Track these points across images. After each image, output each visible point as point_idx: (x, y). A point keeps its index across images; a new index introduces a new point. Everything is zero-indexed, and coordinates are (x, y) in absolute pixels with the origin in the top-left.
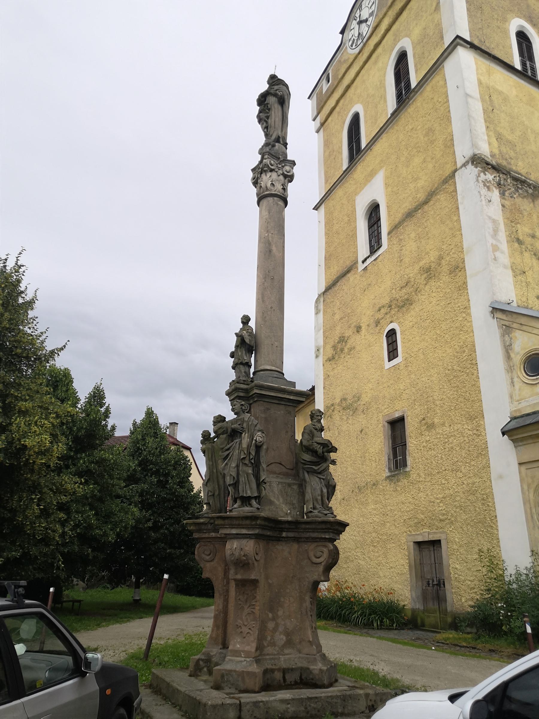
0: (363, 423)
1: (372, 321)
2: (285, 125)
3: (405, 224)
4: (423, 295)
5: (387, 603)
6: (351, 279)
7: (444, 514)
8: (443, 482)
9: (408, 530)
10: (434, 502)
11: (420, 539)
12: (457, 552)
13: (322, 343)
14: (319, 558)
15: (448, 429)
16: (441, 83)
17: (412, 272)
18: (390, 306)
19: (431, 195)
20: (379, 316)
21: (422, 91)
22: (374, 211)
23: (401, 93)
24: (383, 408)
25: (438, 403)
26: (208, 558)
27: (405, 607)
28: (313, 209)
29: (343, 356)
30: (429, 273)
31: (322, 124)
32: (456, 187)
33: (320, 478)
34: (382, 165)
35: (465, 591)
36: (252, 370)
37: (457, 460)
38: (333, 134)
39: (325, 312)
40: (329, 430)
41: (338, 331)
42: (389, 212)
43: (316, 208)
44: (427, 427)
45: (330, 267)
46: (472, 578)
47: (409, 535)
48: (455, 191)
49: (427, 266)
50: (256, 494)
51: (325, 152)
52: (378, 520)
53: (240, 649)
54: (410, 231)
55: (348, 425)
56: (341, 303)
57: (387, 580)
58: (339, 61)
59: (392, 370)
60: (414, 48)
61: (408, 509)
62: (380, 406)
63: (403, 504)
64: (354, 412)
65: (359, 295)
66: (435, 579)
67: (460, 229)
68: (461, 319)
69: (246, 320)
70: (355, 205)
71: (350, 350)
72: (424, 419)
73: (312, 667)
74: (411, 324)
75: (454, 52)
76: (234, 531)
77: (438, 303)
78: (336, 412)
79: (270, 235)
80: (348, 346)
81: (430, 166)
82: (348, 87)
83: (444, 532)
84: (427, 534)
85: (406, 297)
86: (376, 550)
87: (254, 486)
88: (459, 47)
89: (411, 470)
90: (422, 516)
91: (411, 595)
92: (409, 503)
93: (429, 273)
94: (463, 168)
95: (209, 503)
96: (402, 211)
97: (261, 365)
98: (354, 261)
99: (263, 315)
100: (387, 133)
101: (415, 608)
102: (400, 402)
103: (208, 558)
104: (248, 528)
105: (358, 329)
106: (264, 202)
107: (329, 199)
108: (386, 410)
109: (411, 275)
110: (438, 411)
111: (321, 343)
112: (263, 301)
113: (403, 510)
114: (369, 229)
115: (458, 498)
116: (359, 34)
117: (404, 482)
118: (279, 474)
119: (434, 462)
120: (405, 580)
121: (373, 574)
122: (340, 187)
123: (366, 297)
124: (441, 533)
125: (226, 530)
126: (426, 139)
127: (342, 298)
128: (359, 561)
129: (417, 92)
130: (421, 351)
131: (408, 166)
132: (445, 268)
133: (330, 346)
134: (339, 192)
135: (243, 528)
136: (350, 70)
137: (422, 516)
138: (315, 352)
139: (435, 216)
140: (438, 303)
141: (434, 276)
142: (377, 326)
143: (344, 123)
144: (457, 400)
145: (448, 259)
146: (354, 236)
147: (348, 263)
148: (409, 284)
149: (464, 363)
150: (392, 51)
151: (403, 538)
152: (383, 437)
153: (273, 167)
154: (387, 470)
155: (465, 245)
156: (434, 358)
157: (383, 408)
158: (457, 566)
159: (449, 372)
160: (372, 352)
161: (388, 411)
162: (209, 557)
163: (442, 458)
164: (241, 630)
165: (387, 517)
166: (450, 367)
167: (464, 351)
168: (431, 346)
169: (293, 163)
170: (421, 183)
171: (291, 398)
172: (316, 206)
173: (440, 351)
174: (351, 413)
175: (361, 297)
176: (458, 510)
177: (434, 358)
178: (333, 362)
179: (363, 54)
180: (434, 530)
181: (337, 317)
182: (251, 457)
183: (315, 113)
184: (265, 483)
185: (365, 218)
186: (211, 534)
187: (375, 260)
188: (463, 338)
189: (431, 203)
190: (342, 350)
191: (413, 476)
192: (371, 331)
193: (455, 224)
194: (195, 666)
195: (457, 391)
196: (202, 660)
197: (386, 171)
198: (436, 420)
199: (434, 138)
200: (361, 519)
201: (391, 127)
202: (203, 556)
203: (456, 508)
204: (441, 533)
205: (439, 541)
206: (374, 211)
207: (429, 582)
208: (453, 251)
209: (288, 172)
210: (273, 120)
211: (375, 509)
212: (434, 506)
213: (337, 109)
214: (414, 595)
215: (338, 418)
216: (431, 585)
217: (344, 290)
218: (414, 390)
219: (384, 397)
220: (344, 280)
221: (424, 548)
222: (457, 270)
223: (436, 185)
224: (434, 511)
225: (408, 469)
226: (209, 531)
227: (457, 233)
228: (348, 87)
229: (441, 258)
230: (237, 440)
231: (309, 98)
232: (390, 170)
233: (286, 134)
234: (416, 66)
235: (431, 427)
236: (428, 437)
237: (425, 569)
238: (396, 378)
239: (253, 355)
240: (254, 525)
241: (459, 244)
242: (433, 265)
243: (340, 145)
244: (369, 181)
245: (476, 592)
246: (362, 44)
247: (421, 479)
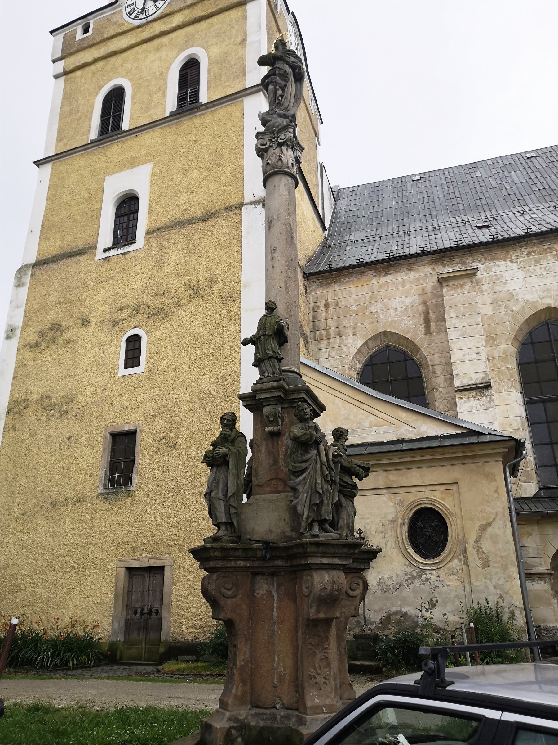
0: (73, 429)
1: (108, 318)
3: (173, 231)
4: (185, 311)
5: (85, 636)
6: (83, 264)
7: (174, 539)
8: (179, 505)
9: (120, 554)
10: (163, 527)
11: (136, 564)
12: (184, 579)
13: (21, 324)
14: (354, 590)
15: (195, 453)
16: (238, 115)
17: (175, 284)
18: (137, 310)
19: (207, 217)
20: (119, 316)
21: (215, 110)
23: (185, 99)
24: (107, 417)
25: (185, 424)
26: (229, 593)
27: (101, 641)
28: (34, 163)
29: (54, 347)
30: (195, 291)
31: (65, 73)
32: (242, 220)
35: (187, 618)
37: (200, 485)
38: (80, 92)
39: (31, 289)
40: (14, 430)
41: (51, 316)
42: (150, 211)
43: (38, 163)
44: (167, 447)
45: (49, 239)
46: (199, 605)
47: (121, 560)
48: (241, 222)
49: (194, 283)
51: (63, 105)
53: (321, 704)
54: (177, 241)
55: (48, 428)
56: (61, 285)
57: (78, 611)
58: (108, 19)
59: (128, 379)
60: (210, 64)
61: (126, 532)
62: (104, 414)
63: (119, 525)
64: (62, 415)
65: (92, 285)
66: (146, 608)
67: (240, 261)
68: (228, 347)
71: (68, 342)
72: (164, 438)
74: (163, 336)
75: (254, 95)
76: (325, 561)
77: (203, 324)
78: (29, 409)
79: (291, 219)
80: (65, 337)
81: (212, 187)
82: (114, 53)
83: (171, 558)
84: (147, 560)
85: (161, 306)
88: (261, 92)
89: (137, 490)
90: (144, 540)
91: (113, 626)
92: (129, 525)
93: (196, 291)
94: (253, 206)
95: (232, 524)
96: (169, 217)
97: (288, 365)
98: (89, 244)
99: (288, 308)
100: (162, 128)
101: (115, 640)
102: (134, 415)
103: (229, 593)
104: (340, 558)
105: (85, 322)
108: (111, 421)
109: (172, 286)
110: (184, 433)
111: (19, 322)
113: (117, 532)
115: (196, 524)
116: (144, 8)
117: (124, 502)
119: (170, 484)
120: (107, 610)
121: (57, 605)
122: (82, 155)
123: (102, 290)
124: (166, 558)
125: (315, 559)
126: (211, 158)
129: (207, 108)
130: (172, 367)
131: (183, 175)
132: (217, 293)
133: (34, 330)
135: (335, 557)
136: (121, 37)
137: (144, 540)
138: (7, 331)
139: (212, 238)
140: (203, 324)
141: (202, 296)
142: (114, 325)
143: (100, 88)
144: (210, 425)
145: (221, 284)
147: (80, 244)
148: (167, 294)
149: (225, 390)
150: (182, 51)
151: (112, 564)
152: (101, 449)
154: (101, 487)
155: (244, 279)
156: (188, 379)
157: (107, 417)
158: (182, 593)
159: (205, 395)
160: (101, 352)
161: (114, 422)
162: (231, 592)
163: (181, 481)
164: (315, 681)
165: (93, 539)
166: (206, 391)
167: (227, 380)
168: (185, 365)
170: (197, 199)
171: (317, 410)
172: (39, 161)
173: (197, 373)
174: (56, 415)
175: (96, 288)
176: (193, 536)
177: (188, 379)
178: (36, 351)
179: (143, 31)
180: (157, 556)
181: (52, 299)
183: (59, 55)
186: (239, 562)
187: (123, 254)
188: (227, 366)
189: (209, 223)
190: (54, 340)
191: (139, 496)
192: (105, 329)
193: (235, 254)
194: (225, 738)
195: (212, 417)
196: (234, 728)
197: (154, 166)
198: (180, 441)
199: (221, 162)
201: (169, 126)
202: (223, 590)
203: (191, 534)
204: (166, 558)
205: (161, 569)
207: (136, 610)
208: (229, 279)
211: (75, 530)
212: (163, 531)
213: (93, 68)
214: (116, 626)
215: (33, 418)
216: (139, 614)
217: (69, 272)
218: (155, 405)
219: (112, 405)
220: (70, 261)
221: (136, 575)
222: (231, 299)
223: (217, 208)
224: (162, 535)
225: (132, 488)
226: (237, 558)
227: (236, 264)
228: (114, 53)
229: (212, 281)
231: (51, 32)
232: (160, 169)
234: (209, 82)
235: (172, 447)
236: (167, 458)
237: (134, 597)
238: (132, 388)
240: (351, 554)
241: (237, 275)
242: (202, 286)
243: (90, 110)
245: (201, 619)
246: (144, 21)
247: (149, 501)
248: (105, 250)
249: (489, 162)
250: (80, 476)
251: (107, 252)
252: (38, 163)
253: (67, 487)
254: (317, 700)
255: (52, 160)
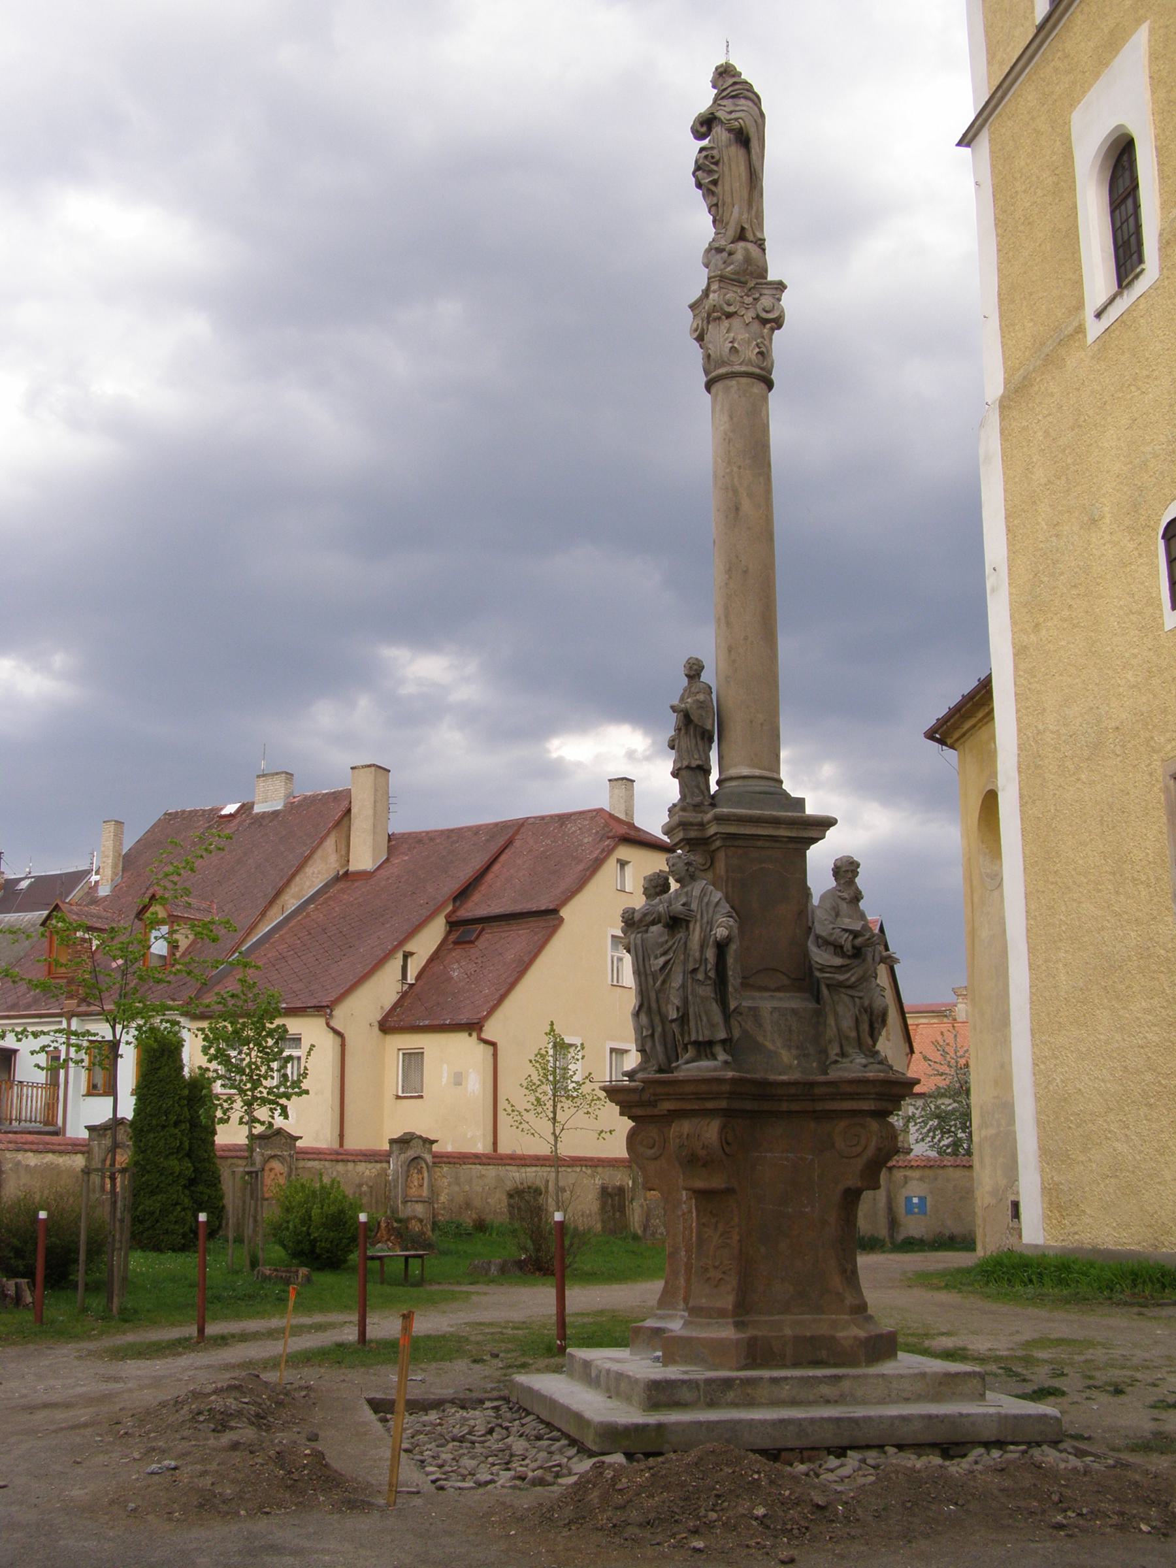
2: (756, 193)
22: (1121, 156)
28: (959, 144)
33: (852, 997)
34: (1141, 12)
36: (714, 777)
43: (966, 141)
45: (1013, 325)
50: (722, 1035)
52: (1156, 1039)
55: (1079, 785)
69: (694, 671)
70: (1069, 138)
73: (840, 1334)
86: (1155, 1115)
87: (718, 1018)
106: (718, 387)
107: (1000, 115)
112: (728, 624)
114: (1112, 212)
118: (778, 989)
121: (1149, 1176)
127: (1050, 419)
128: (1117, 1144)
134: (1025, 97)
146: (1070, 236)
152: (1164, 819)
153: (731, 309)
162: (653, 1151)
169: (780, 286)
172: (965, 135)
182: (709, 966)
184: (741, 1014)
185: (1102, 168)
200: (1118, 1037)
206: (1121, 156)
209: (767, 312)
210: (727, 188)
211: (1147, 1011)
230: (681, 935)
233: (759, 216)
239: (715, 746)
244: (1107, 65)
248: (1098, 315)
249: (1159, 143)
250: (1141, 887)
251: (1104, 316)
252: (966, 141)
253: (1126, 917)
254: (704, 1300)
255: (986, 120)
